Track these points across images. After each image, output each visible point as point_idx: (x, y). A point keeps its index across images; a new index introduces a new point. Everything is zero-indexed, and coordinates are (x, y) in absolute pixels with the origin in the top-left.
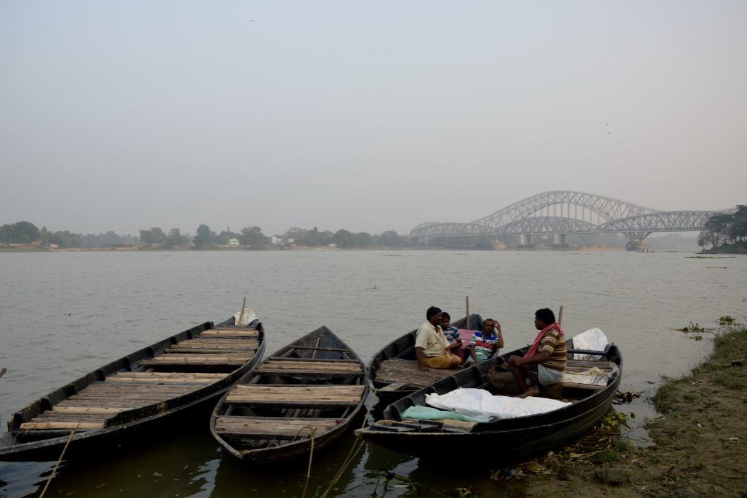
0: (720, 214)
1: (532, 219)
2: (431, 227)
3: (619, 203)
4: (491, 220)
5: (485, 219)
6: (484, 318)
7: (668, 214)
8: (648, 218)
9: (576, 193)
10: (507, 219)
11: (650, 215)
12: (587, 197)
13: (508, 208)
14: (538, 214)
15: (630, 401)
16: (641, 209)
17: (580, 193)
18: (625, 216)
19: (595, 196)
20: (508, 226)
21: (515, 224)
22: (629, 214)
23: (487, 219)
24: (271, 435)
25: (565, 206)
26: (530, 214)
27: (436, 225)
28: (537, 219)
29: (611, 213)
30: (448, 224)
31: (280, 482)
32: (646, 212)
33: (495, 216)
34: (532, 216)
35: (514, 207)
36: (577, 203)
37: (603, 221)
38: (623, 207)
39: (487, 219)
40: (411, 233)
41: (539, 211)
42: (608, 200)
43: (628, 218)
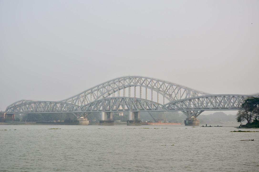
1: (111, 99)
3: (179, 87)
5: (72, 98)
9: (146, 78)
14: (116, 95)
16: (195, 92)
18: (183, 97)
20: (91, 104)
25: (138, 88)
26: (109, 95)
27: (30, 103)
32: (200, 95)
34: (111, 96)
35: (90, 91)
36: (147, 86)
37: (167, 101)
38: (182, 90)
42: (171, 84)
43: (186, 100)
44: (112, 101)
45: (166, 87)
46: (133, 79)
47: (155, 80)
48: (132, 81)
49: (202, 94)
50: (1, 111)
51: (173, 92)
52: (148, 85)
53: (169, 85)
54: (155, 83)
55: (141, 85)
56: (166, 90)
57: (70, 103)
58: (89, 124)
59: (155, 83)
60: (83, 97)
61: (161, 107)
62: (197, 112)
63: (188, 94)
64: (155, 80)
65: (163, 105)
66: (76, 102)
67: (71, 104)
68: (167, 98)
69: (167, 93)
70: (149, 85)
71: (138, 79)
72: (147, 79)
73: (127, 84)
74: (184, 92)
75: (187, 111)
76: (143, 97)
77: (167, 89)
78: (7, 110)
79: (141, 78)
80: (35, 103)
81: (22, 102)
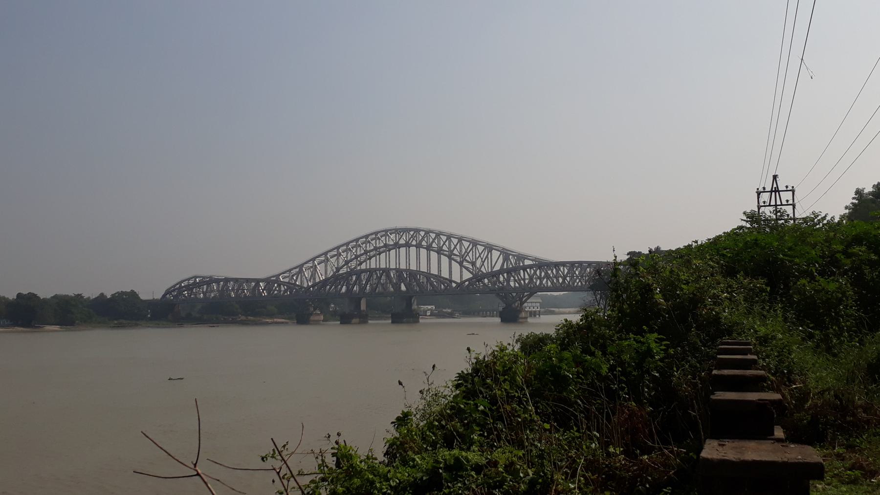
0: (136, 325)
3: (490, 248)
4: (297, 274)
5: (290, 270)
6: (842, 214)
7: (557, 265)
9: (428, 232)
11: (530, 267)
14: (373, 264)
15: (535, 316)
16: (521, 257)
17: (423, 231)
19: (423, 231)
21: (337, 279)
22: (503, 264)
23: (294, 271)
24: (531, 296)
25: (413, 250)
28: (371, 271)
32: (527, 262)
34: (363, 266)
35: (322, 258)
36: (429, 248)
37: (467, 275)
38: (495, 254)
42: (475, 243)
44: (364, 277)
45: (480, 252)
46: (403, 234)
47: (434, 233)
48: (402, 236)
49: (532, 260)
50: (2, 295)
51: (478, 257)
52: (443, 246)
53: (500, 254)
54: (455, 244)
55: (419, 246)
56: (465, 253)
57: (287, 280)
58: (359, 323)
59: (455, 244)
60: (312, 269)
61: (455, 287)
62: (523, 295)
63: (506, 259)
64: (432, 232)
65: (459, 282)
66: (297, 278)
67: (289, 283)
68: (467, 269)
69: (467, 258)
70: (434, 245)
71: (412, 233)
72: (439, 235)
73: (391, 243)
74: (499, 256)
75: (503, 293)
76: (424, 269)
77: (468, 252)
78: (164, 296)
79: (417, 231)
80: (217, 281)
81: (195, 280)
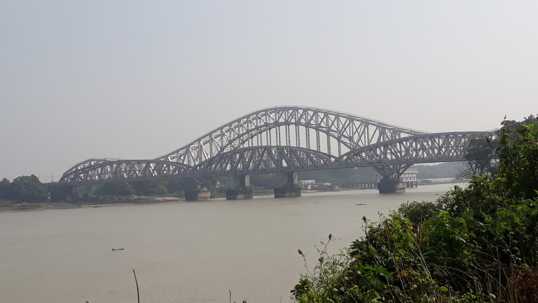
1: (245, 150)
2: (94, 168)
3: (366, 123)
7: (432, 137)
8: (343, 120)
10: (208, 152)
11: (406, 139)
12: (357, 124)
13: (210, 134)
14: (255, 142)
16: (396, 131)
17: (301, 109)
18: (374, 141)
19: (301, 109)
20: (210, 161)
21: (221, 157)
23: (181, 152)
25: (292, 127)
26: (243, 143)
27: (103, 164)
28: (253, 150)
29: (356, 139)
30: (119, 162)
31: (294, 176)
32: (403, 135)
33: (192, 146)
34: (246, 145)
36: (308, 125)
37: (345, 150)
38: (372, 128)
39: (181, 152)
40: (62, 179)
41: (247, 142)
43: (378, 145)
